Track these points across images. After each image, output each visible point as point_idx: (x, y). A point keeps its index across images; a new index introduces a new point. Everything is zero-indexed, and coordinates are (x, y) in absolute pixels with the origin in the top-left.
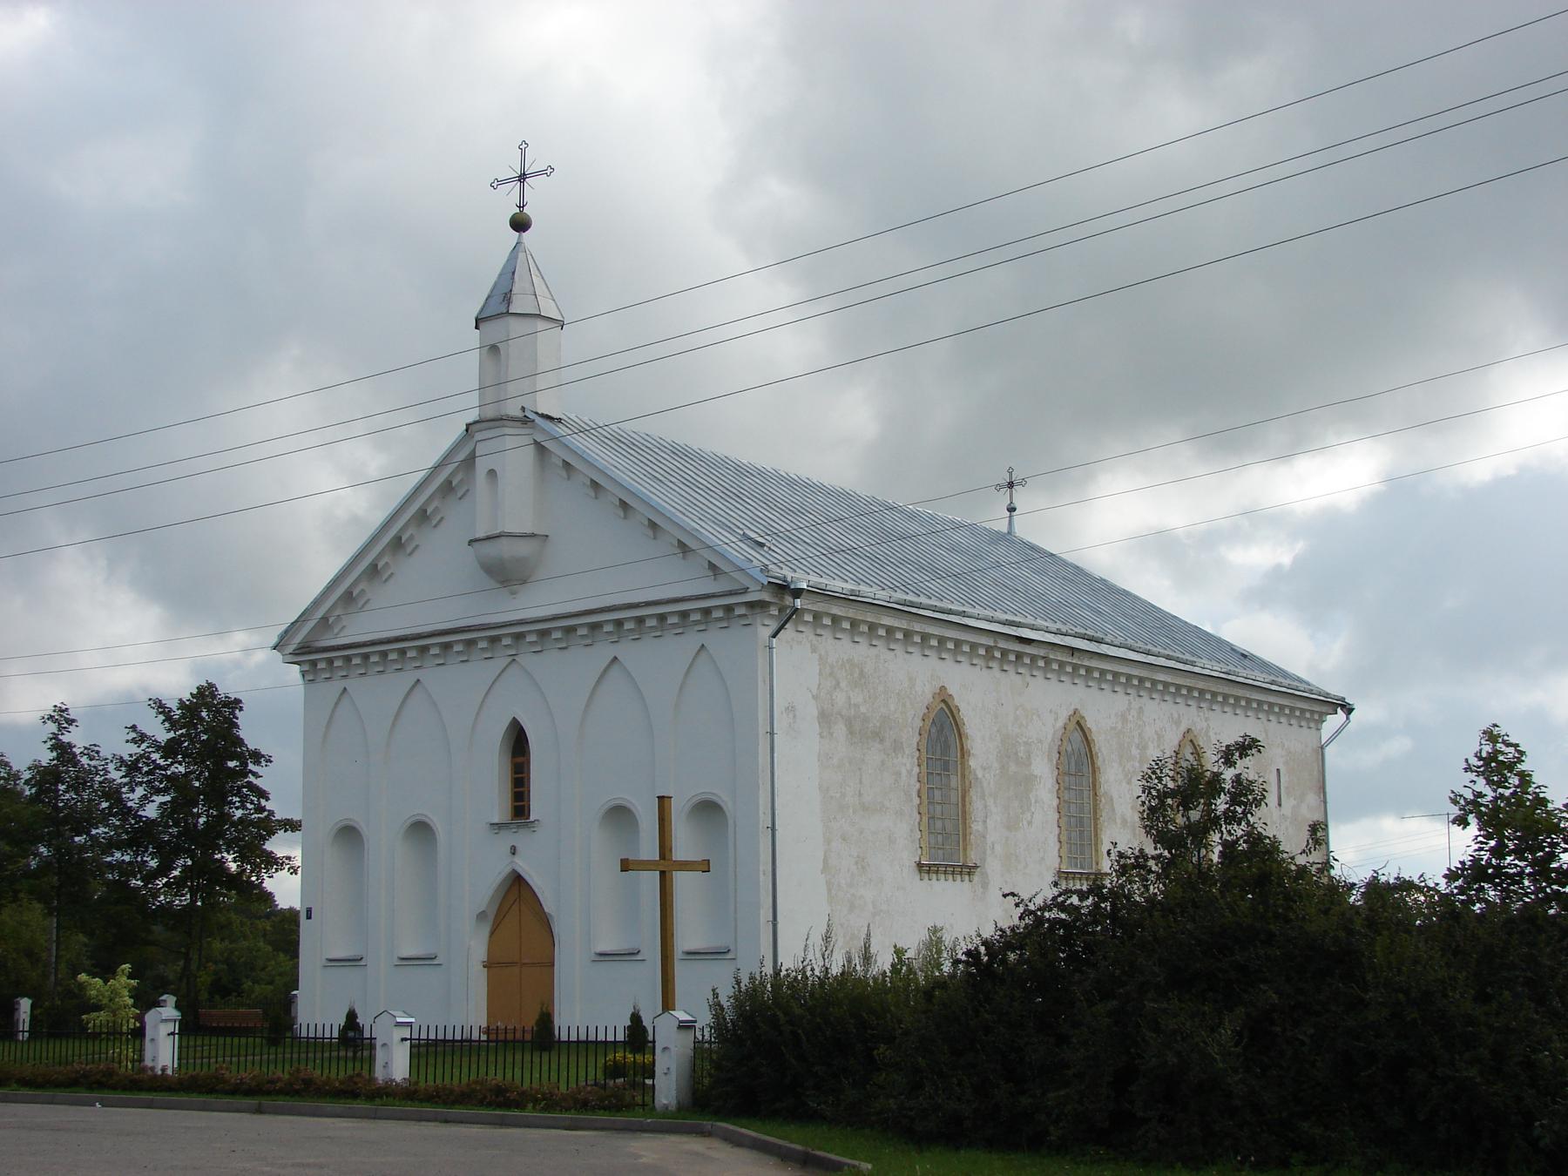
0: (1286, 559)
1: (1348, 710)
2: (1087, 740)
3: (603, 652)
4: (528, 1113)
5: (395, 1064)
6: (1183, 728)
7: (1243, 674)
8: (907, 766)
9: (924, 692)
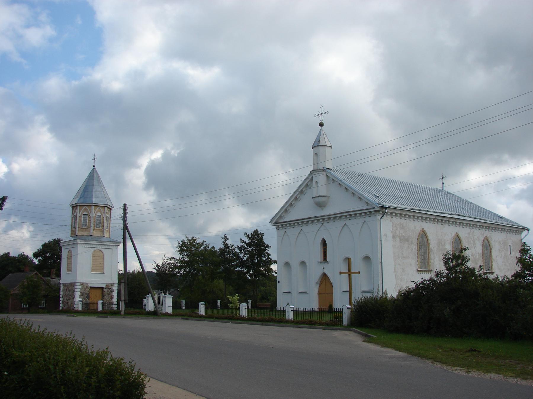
0: (525, 187)
1: (528, 230)
2: (460, 240)
3: (342, 222)
4: (316, 326)
5: (290, 316)
6: (485, 236)
7: (500, 222)
8: (414, 247)
9: (418, 230)
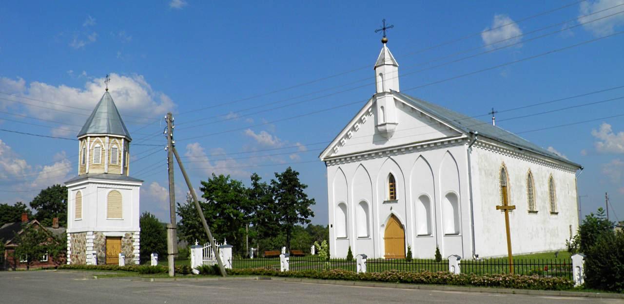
5: (361, 268)
6: (550, 173)
